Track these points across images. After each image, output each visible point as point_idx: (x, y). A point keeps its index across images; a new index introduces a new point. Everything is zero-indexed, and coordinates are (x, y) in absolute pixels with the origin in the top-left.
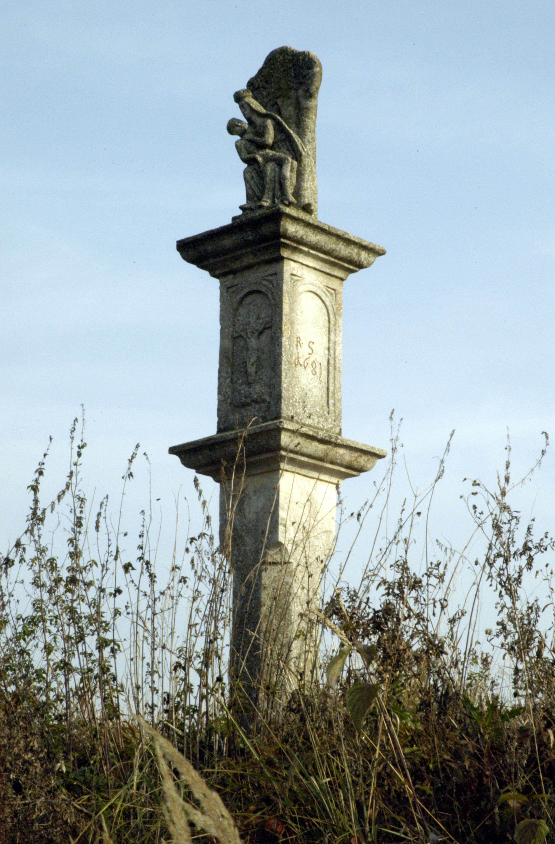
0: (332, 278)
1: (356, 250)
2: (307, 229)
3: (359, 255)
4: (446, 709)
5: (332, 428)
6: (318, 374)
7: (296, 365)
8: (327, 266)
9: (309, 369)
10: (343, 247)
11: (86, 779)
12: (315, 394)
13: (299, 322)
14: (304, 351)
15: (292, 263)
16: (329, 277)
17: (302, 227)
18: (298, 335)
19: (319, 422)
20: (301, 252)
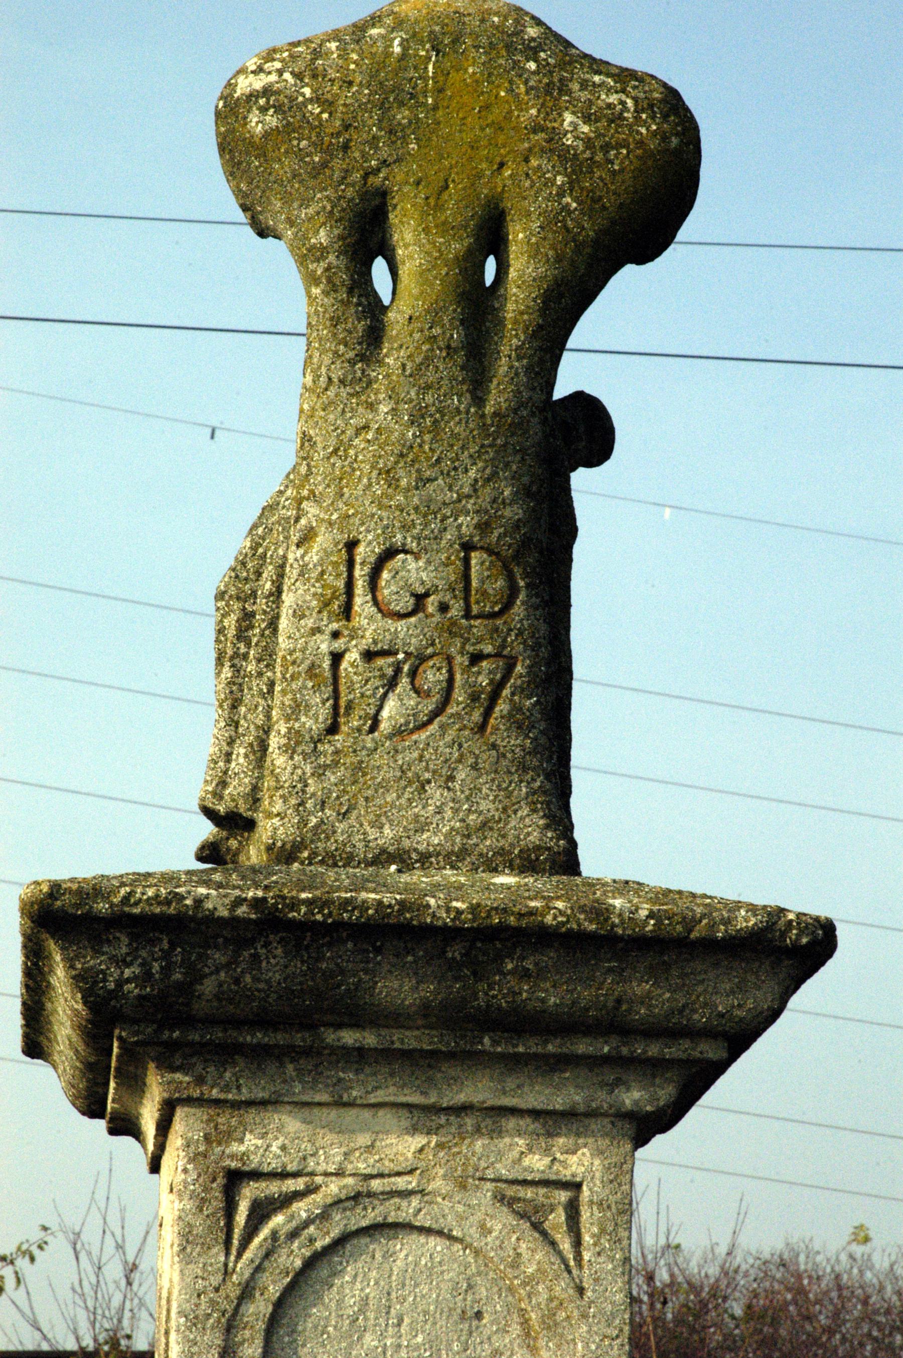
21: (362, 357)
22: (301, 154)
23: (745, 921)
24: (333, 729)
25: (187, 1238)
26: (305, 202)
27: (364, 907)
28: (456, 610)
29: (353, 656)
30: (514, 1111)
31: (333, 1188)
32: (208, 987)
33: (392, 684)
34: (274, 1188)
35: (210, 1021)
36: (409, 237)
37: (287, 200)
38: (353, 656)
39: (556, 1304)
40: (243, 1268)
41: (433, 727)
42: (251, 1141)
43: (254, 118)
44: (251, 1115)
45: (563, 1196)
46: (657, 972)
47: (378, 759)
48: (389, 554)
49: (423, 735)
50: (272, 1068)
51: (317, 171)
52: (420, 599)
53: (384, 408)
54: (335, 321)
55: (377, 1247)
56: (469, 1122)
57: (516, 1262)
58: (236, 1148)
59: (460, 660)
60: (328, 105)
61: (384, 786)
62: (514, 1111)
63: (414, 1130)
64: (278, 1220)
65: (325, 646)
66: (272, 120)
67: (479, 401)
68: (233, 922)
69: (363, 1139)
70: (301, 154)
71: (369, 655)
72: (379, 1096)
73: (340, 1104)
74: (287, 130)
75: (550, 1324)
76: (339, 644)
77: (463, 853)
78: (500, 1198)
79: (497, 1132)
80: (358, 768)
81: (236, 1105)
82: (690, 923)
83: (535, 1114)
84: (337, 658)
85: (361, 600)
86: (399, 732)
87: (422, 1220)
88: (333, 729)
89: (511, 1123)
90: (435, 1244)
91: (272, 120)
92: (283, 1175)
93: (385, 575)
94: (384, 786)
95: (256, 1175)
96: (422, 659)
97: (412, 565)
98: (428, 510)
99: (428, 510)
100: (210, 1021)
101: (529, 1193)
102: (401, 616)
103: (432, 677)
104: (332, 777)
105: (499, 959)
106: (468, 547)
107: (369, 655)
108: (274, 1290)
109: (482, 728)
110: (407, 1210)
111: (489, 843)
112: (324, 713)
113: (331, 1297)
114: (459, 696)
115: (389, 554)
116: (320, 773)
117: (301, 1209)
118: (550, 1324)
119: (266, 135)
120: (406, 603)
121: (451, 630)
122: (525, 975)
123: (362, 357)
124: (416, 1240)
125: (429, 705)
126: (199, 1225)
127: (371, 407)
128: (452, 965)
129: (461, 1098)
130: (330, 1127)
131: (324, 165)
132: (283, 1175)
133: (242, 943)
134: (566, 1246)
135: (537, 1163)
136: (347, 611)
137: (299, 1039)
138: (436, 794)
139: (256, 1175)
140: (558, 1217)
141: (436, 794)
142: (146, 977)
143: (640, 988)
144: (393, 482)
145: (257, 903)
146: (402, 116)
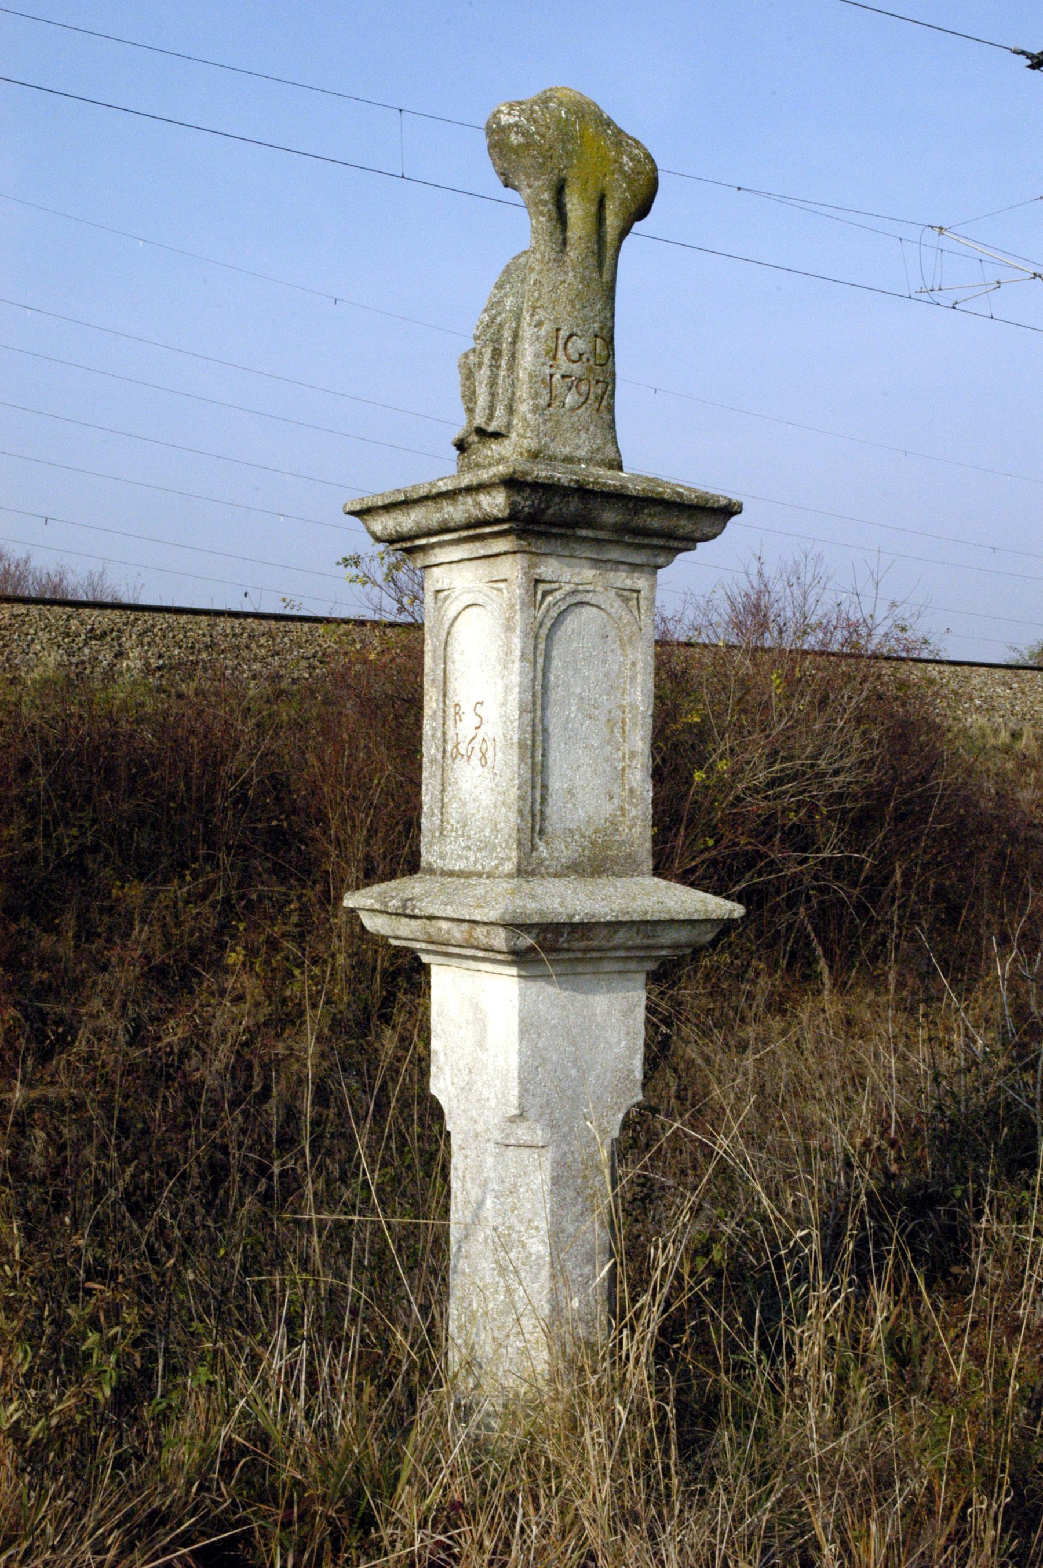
0: (500, 559)
1: (469, 500)
2: (393, 515)
3: (478, 504)
4: (840, 1557)
5: (497, 867)
6: (489, 764)
7: (454, 759)
8: (478, 544)
9: (475, 760)
10: (451, 509)
11: (171, 1391)
12: (484, 803)
13: (457, 674)
14: (463, 729)
15: (435, 569)
16: (492, 560)
17: (386, 516)
18: (456, 699)
19: (476, 862)
20: (432, 546)
21: (561, 251)
22: (534, 157)
23: (723, 502)
24: (549, 405)
25: (523, 604)
26: (537, 179)
27: (609, 486)
28: (592, 362)
29: (557, 376)
30: (622, 563)
31: (567, 588)
32: (551, 511)
33: (570, 389)
34: (548, 587)
35: (545, 523)
36: (575, 201)
37: (528, 176)
38: (557, 376)
39: (633, 634)
40: (539, 615)
41: (583, 409)
42: (543, 569)
43: (513, 137)
44: (543, 558)
45: (635, 595)
46: (690, 518)
47: (565, 419)
48: (571, 336)
49: (579, 411)
50: (553, 541)
51: (542, 166)
52: (581, 355)
53: (571, 274)
54: (551, 234)
55: (577, 610)
56: (609, 565)
57: (620, 619)
58: (538, 571)
59: (593, 382)
60: (543, 136)
61: (566, 430)
62: (622, 563)
63: (592, 568)
64: (549, 599)
65: (548, 371)
66: (521, 139)
67: (601, 276)
68: (569, 487)
69: (577, 570)
70: (534, 157)
71: (563, 377)
72: (584, 555)
73: (572, 556)
74: (528, 145)
75: (631, 642)
76: (553, 371)
77: (591, 460)
78: (617, 594)
79: (617, 570)
80: (558, 422)
81: (538, 554)
82: (707, 500)
83: (630, 564)
84: (551, 376)
85: (560, 353)
86: (572, 409)
87: (593, 602)
88: (549, 405)
89: (622, 567)
90: (595, 610)
91: (521, 139)
92: (550, 582)
93: (570, 344)
94: (566, 430)
95: (543, 581)
96: (580, 380)
97: (579, 341)
98: (585, 319)
99: (585, 319)
100: (545, 523)
101: (625, 593)
102: (574, 362)
103: (584, 388)
104: (549, 425)
105: (643, 509)
106: (596, 336)
107: (563, 377)
108: (549, 625)
109: (598, 410)
110: (588, 598)
111: (599, 457)
112: (547, 398)
113: (563, 628)
114: (592, 397)
115: (571, 336)
116: (545, 422)
117: (558, 595)
118: (631, 642)
119: (519, 145)
120: (575, 357)
121: (590, 369)
122: (650, 515)
123: (561, 251)
124: (589, 608)
125: (582, 399)
126: (527, 599)
127: (566, 273)
128: (628, 509)
129: (610, 557)
130: (568, 565)
131: (544, 163)
132: (550, 582)
133: (565, 496)
134: (636, 613)
135: (628, 583)
136: (555, 357)
137: (569, 532)
138: (583, 434)
139: (543, 581)
140: (634, 603)
141: (583, 434)
142: (532, 506)
143: (683, 522)
144: (574, 306)
145: (577, 481)
146: (570, 147)
